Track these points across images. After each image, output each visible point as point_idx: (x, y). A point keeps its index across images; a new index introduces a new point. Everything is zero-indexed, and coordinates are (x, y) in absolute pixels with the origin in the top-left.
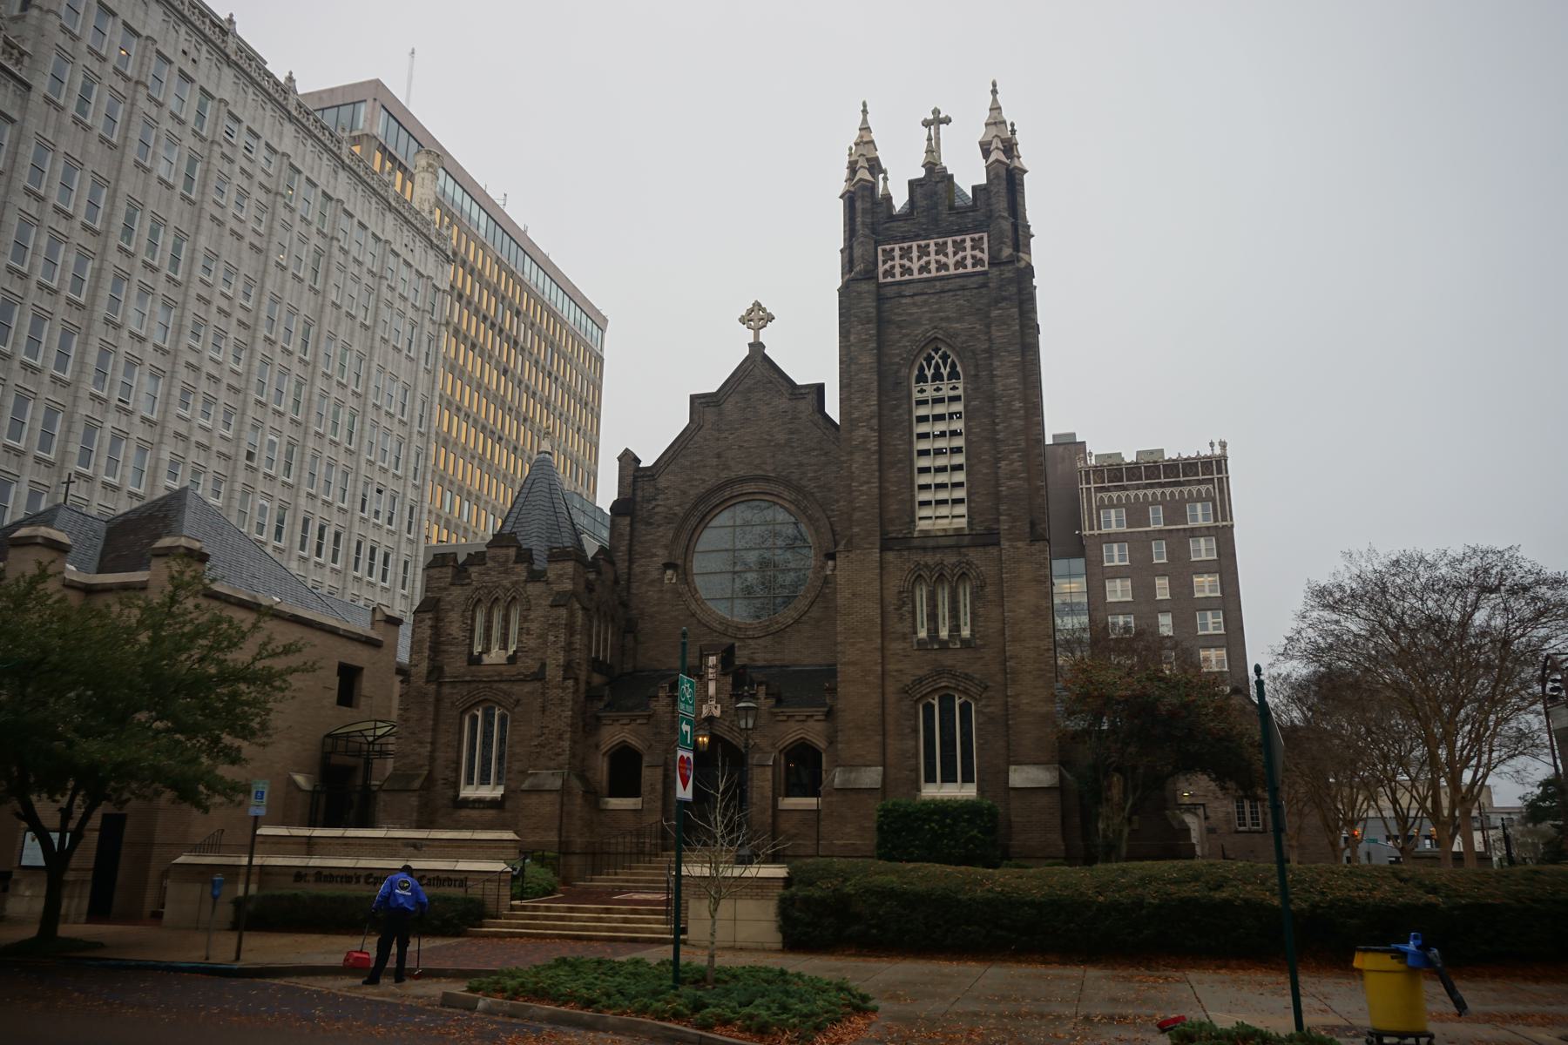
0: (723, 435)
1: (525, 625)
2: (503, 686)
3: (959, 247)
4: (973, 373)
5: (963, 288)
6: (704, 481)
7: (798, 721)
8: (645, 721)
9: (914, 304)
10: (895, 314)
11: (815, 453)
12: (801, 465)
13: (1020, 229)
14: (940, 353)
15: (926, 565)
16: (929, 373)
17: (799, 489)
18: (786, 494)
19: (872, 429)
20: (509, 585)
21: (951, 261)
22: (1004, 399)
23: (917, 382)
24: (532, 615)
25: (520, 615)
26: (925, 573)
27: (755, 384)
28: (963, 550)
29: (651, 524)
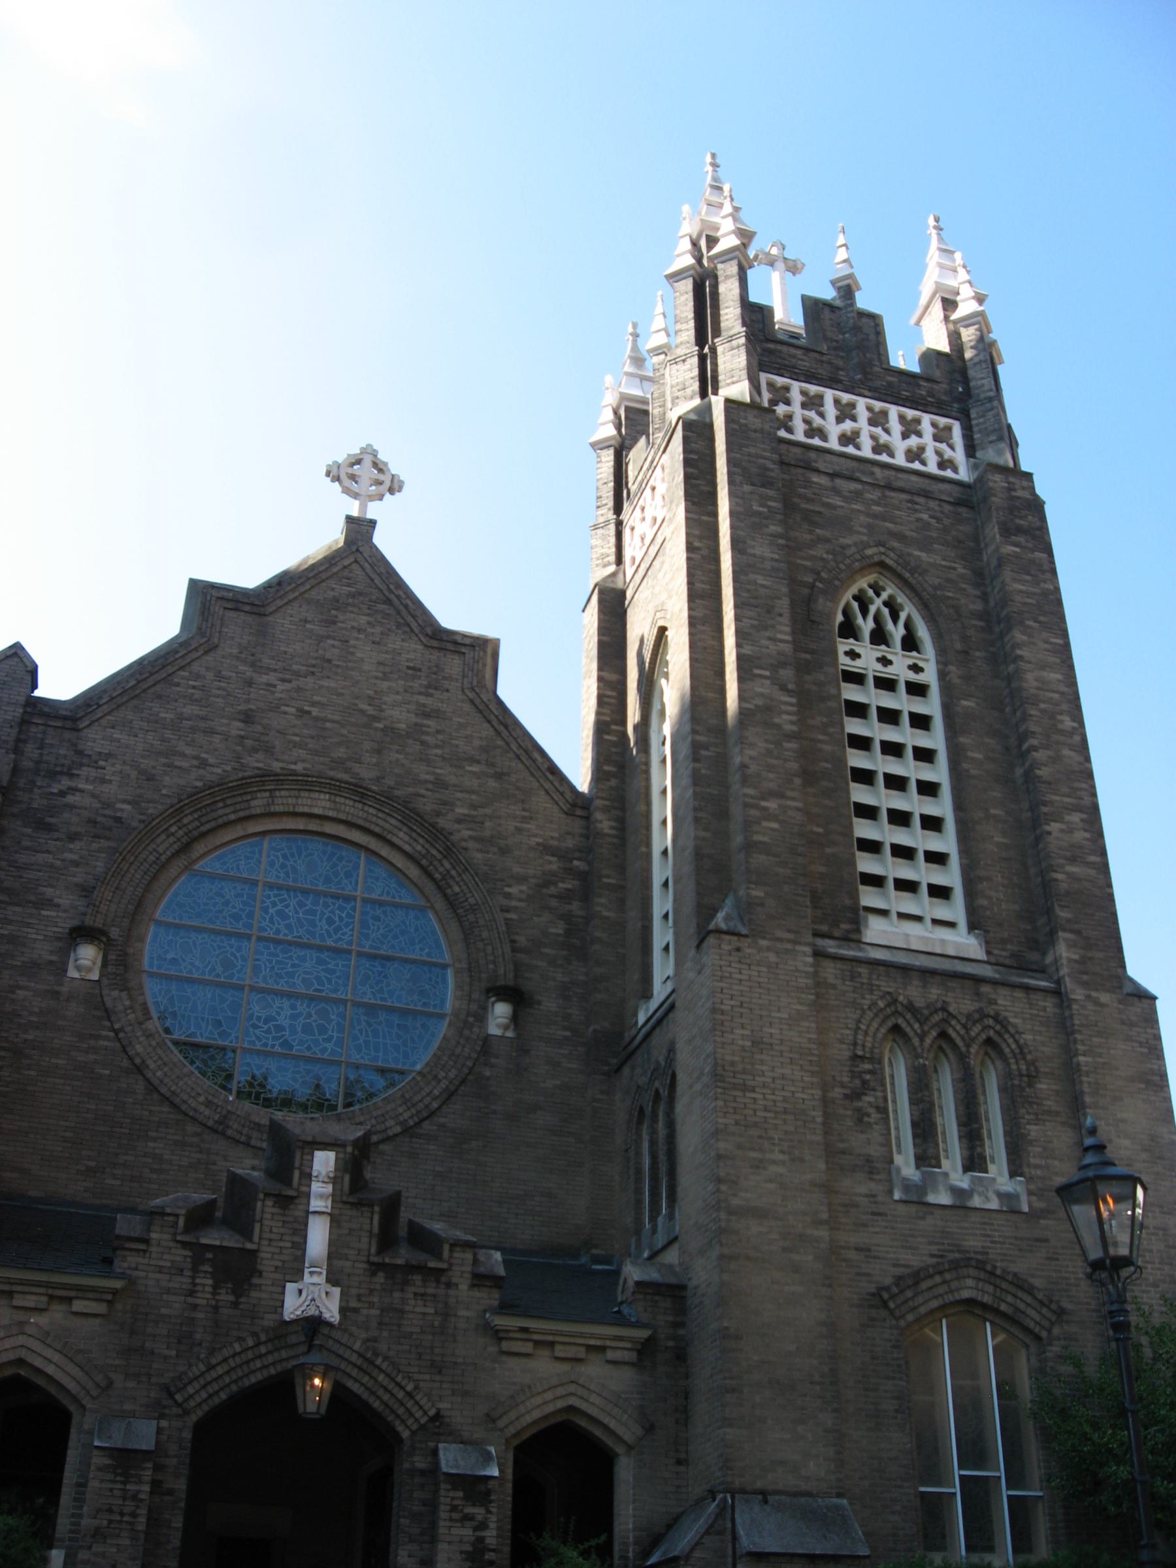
0: (264, 679)
5: (926, 495)
6: (204, 764)
7: (608, 1362)
8: (101, 1308)
10: (800, 496)
11: (475, 768)
12: (440, 784)
15: (911, 1007)
17: (436, 834)
18: (402, 838)
19: (783, 688)
22: (1042, 706)
26: (912, 1028)
28: (985, 989)
29: (49, 828)
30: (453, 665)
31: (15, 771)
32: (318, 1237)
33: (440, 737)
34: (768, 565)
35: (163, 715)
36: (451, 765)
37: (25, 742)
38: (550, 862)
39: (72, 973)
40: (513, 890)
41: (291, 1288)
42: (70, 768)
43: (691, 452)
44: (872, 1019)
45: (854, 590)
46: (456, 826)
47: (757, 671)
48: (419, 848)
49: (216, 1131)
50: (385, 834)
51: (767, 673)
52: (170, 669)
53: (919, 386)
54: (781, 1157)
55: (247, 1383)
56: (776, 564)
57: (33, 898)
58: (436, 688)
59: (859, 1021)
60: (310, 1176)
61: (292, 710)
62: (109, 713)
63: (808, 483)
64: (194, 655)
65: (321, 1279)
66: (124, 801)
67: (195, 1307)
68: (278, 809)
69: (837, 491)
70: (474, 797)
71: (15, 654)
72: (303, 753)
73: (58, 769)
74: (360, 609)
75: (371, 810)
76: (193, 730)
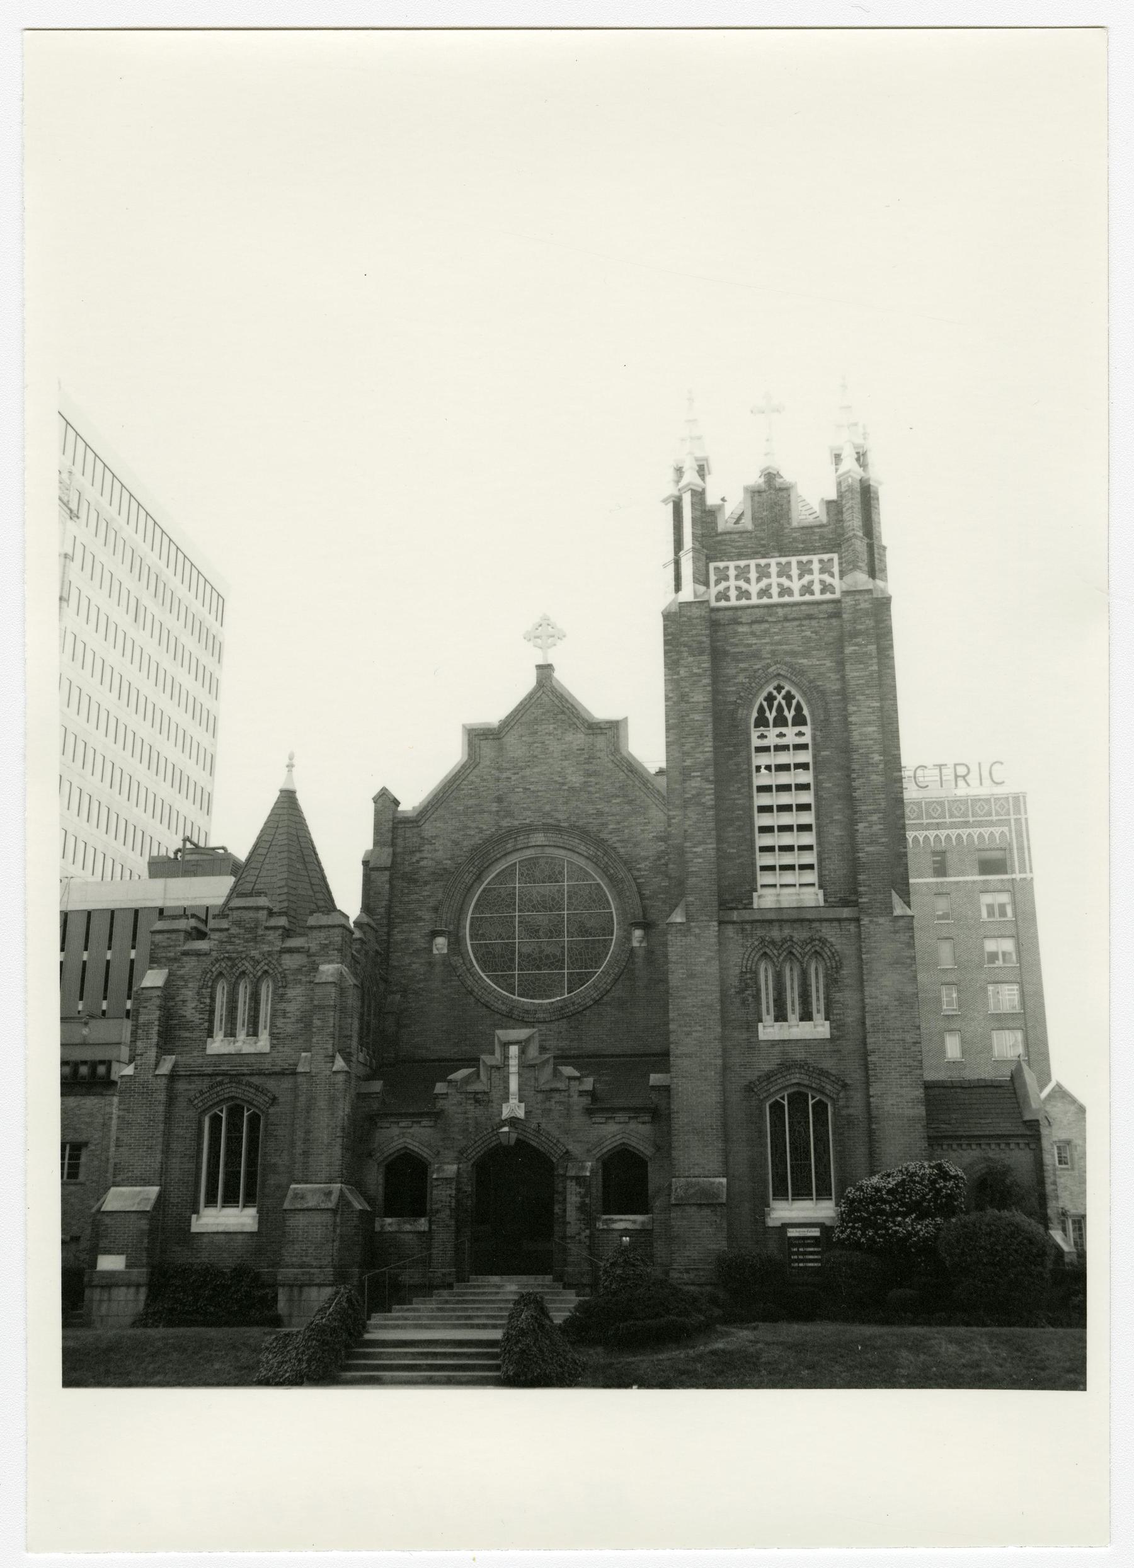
0: (505, 775)
1: (283, 1006)
2: (255, 1080)
3: (805, 570)
4: (822, 718)
5: (810, 617)
6: (481, 831)
9: (753, 634)
11: (618, 800)
12: (600, 814)
13: (876, 551)
14: (783, 692)
15: (773, 942)
16: (771, 716)
17: (600, 843)
18: (582, 848)
19: (708, 781)
20: (258, 956)
21: (754, 588)
22: (861, 751)
23: (757, 726)
24: (291, 993)
25: (274, 993)
27: (543, 714)
30: (601, 742)
31: (394, 854)
32: (514, 1084)
33: (598, 786)
34: (701, 706)
35: (458, 808)
36: (605, 802)
37: (396, 838)
38: (661, 846)
39: (435, 952)
40: (642, 866)
41: (504, 1105)
42: (419, 847)
43: (669, 635)
44: (752, 952)
45: (765, 694)
46: (610, 836)
47: (693, 774)
48: (591, 853)
49: (508, 1017)
50: (574, 849)
51: (699, 774)
52: (458, 782)
53: (814, 533)
54: (700, 1028)
55: (490, 1146)
56: (705, 705)
57: (411, 918)
58: (593, 759)
59: (744, 954)
60: (508, 1058)
61: (521, 790)
62: (433, 814)
63: (736, 633)
64: (469, 771)
65: (516, 1101)
66: (446, 859)
67: (467, 1118)
68: (519, 847)
69: (753, 634)
70: (618, 817)
71: (384, 794)
72: (529, 813)
73: (414, 849)
74: (549, 720)
75: (566, 837)
76: (474, 812)
